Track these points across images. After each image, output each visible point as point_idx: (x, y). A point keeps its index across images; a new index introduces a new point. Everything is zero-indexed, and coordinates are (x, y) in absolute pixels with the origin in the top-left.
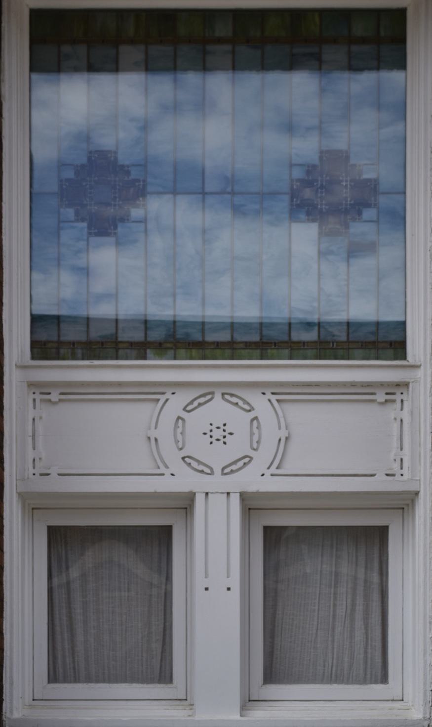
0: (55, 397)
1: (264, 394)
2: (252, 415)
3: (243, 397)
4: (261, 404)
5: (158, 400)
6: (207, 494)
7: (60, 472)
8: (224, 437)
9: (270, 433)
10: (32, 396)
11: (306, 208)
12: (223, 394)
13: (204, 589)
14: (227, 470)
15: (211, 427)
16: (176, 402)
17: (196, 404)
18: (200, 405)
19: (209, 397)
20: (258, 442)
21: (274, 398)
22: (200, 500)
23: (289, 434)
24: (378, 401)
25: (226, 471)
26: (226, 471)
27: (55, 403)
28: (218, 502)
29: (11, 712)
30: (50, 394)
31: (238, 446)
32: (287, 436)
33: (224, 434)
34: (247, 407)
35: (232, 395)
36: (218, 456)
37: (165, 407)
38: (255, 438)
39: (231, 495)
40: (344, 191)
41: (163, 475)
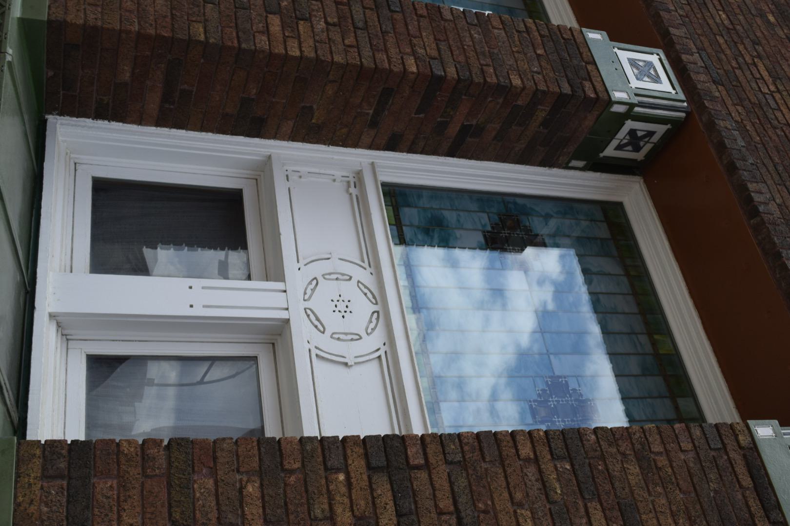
0: (352, 190)
1: (384, 344)
2: (363, 334)
3: (378, 325)
4: (375, 341)
5: (363, 262)
6: (285, 291)
7: (291, 189)
8: (338, 301)
9: (350, 351)
10: (381, 345)
11: (547, 388)
12: (378, 312)
13: (194, 306)
14: (309, 312)
15: (346, 301)
16: (364, 276)
17: (366, 291)
18: (365, 294)
19: (374, 301)
20: (338, 339)
21: (381, 353)
22: (280, 285)
23: (351, 366)
24: (350, 189)
25: (308, 312)
26: (308, 312)
27: (347, 191)
28: (279, 300)
29: (62, 124)
30: (355, 187)
31: (333, 323)
32: (349, 364)
33: (341, 301)
34: (369, 331)
35: (378, 319)
36: (321, 303)
37: (355, 265)
38: (342, 337)
39: (287, 311)
40: (570, 419)
41: (298, 262)
